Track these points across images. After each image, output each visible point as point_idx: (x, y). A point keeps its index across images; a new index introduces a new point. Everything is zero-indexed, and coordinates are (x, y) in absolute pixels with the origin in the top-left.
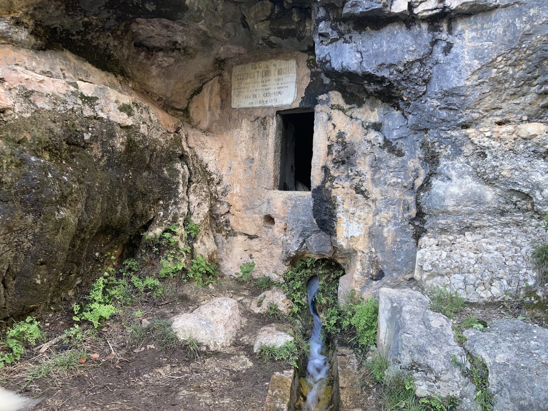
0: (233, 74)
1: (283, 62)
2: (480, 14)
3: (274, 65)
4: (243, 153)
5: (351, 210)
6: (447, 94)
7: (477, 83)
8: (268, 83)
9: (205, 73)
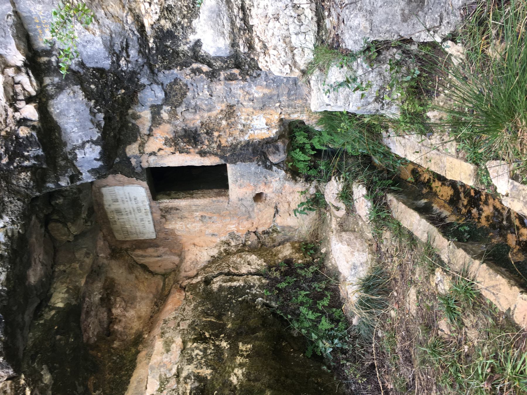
0: (124, 240)
1: (105, 198)
2: (26, 27)
3: (110, 205)
4: (197, 226)
5: (240, 127)
6: (112, 52)
7: (96, 23)
8: (127, 210)
9: (127, 265)
